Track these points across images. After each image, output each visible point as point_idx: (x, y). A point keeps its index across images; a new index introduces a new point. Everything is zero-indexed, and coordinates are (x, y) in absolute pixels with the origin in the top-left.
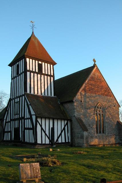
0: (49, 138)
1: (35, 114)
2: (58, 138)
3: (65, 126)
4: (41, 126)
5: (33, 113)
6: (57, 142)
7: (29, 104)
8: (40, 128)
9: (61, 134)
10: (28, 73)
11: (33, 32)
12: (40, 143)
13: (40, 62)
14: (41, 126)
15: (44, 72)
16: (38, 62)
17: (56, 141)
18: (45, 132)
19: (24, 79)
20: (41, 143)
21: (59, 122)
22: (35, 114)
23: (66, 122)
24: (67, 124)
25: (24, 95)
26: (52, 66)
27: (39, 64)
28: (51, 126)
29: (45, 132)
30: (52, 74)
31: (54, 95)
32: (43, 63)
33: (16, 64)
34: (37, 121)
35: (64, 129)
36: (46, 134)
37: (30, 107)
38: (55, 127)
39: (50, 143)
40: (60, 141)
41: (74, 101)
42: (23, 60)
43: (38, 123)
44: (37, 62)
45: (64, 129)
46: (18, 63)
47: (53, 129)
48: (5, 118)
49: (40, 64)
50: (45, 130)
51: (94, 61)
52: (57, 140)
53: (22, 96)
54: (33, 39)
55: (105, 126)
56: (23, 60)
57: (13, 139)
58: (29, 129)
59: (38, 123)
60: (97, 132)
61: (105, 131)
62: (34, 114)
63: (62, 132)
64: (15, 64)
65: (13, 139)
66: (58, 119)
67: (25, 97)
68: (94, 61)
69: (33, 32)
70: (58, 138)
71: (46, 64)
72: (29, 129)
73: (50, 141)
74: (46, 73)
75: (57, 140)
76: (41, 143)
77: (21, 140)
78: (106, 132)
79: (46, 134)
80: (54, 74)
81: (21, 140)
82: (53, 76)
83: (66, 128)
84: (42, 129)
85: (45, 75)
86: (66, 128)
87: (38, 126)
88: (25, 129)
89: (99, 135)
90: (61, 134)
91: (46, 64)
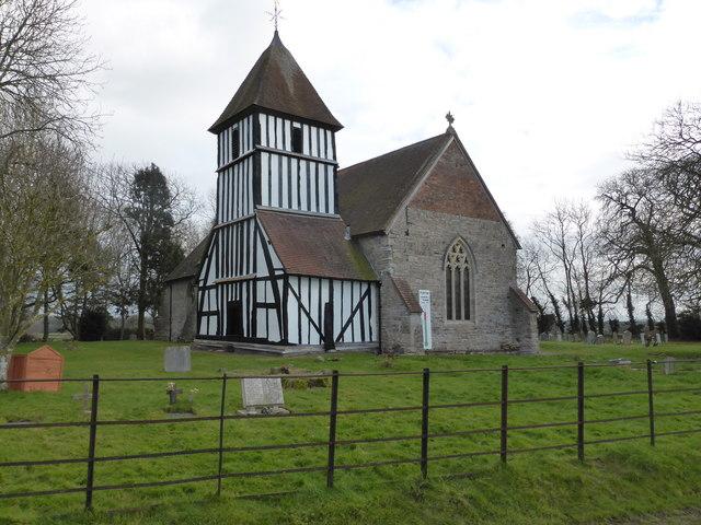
0: (319, 330)
2: (343, 330)
3: (362, 299)
4: (299, 299)
5: (276, 264)
7: (267, 239)
9: (351, 320)
10: (264, 156)
11: (276, 33)
14: (299, 299)
17: (338, 339)
18: (308, 315)
23: (364, 289)
24: (368, 292)
25: (255, 217)
26: (329, 133)
28: (325, 299)
29: (308, 315)
30: (330, 157)
35: (360, 306)
36: (310, 320)
42: (251, 117)
45: (360, 306)
46: (235, 126)
47: (330, 307)
48: (202, 276)
49: (297, 129)
51: (450, 118)
52: (341, 335)
56: (251, 117)
58: (267, 306)
60: (450, 317)
63: (353, 313)
67: (257, 227)
69: (276, 33)
70: (343, 330)
72: (267, 306)
73: (321, 337)
75: (341, 335)
79: (310, 320)
80: (335, 157)
83: (365, 302)
84: (301, 306)
85: (308, 160)
86: (365, 302)
87: (291, 297)
88: (257, 305)
90: (351, 320)
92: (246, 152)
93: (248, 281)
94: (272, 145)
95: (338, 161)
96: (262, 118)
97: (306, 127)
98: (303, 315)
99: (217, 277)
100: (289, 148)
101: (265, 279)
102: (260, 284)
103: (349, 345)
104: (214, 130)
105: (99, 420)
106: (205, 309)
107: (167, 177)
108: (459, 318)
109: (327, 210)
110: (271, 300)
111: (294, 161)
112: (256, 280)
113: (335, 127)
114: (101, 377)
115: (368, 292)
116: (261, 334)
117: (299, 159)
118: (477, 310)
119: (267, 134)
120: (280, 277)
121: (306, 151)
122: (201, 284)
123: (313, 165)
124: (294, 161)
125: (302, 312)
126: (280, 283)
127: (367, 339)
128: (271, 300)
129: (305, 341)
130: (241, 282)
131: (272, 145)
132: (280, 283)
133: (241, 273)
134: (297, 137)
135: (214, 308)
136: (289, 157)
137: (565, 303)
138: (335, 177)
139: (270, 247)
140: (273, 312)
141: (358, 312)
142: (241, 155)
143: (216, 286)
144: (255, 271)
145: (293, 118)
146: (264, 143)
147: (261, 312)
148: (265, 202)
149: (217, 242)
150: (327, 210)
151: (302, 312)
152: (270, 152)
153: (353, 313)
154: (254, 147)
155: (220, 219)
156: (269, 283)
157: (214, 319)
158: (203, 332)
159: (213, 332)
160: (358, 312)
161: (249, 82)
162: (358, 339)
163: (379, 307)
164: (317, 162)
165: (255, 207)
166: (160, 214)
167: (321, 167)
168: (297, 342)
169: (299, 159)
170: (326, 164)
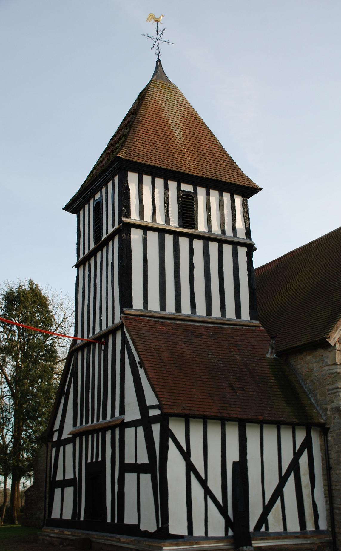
0: (223, 510)
1: (158, 403)
2: (267, 509)
3: (297, 455)
4: (186, 455)
5: (151, 399)
6: (263, 529)
7: (137, 360)
8: (182, 464)
9: (279, 493)
10: (136, 236)
11: (159, 62)
13: (187, 188)
14: (186, 455)
16: (179, 188)
17: (258, 527)
18: (203, 483)
19: (95, 229)
22: (158, 403)
23: (301, 437)
24: (307, 444)
25: (120, 327)
26: (238, 200)
28: (233, 456)
29: (203, 483)
30: (241, 235)
31: (252, 317)
32: (202, 192)
33: (92, 202)
34: (166, 434)
35: (294, 466)
36: (208, 493)
37: (141, 372)
38: (248, 457)
39: (230, 533)
41: (332, 343)
42: (116, 179)
43: (171, 443)
44: (173, 185)
45: (294, 466)
46: (97, 196)
48: (57, 426)
49: (187, 193)
50: (203, 477)
52: (263, 520)
53: (113, 331)
54: (156, 94)
56: (116, 179)
58: (138, 469)
59: (171, 443)
62: (155, 402)
63: (283, 480)
64: (88, 202)
65: (82, 519)
66: (262, 423)
67: (124, 342)
69: (159, 62)
70: (267, 509)
71: (211, 192)
72: (138, 469)
73: (228, 524)
75: (263, 520)
77: (109, 520)
79: (208, 493)
80: (248, 234)
81: (109, 520)
82: (251, 249)
83: (304, 460)
84: (190, 468)
85: (206, 239)
86: (304, 460)
87: (173, 453)
88: (126, 468)
90: (279, 493)
91: (211, 192)
92: (111, 230)
93: (112, 428)
94: (148, 218)
95: (255, 239)
96: (132, 178)
97: (201, 192)
98: (195, 483)
99: (75, 425)
100: (174, 224)
101: (134, 424)
102: (129, 432)
103: (277, 536)
104: (67, 208)
106: (59, 477)
107: (50, 297)
109: (238, 314)
110: (143, 459)
111: (184, 242)
112: (123, 425)
113: (236, 163)
115: (307, 444)
116: (130, 518)
117: (191, 237)
119: (141, 201)
120: (155, 419)
121: (202, 227)
122: (55, 438)
123: (213, 247)
124: (184, 242)
126: (156, 428)
127: (310, 527)
128: (143, 459)
129: (199, 531)
130: (103, 430)
131: (148, 218)
132: (156, 428)
133: (104, 417)
135: (70, 476)
136: (176, 235)
138: (249, 275)
139: (141, 372)
140: (146, 479)
141: (306, 453)
142: (104, 236)
143: (71, 440)
144: (122, 412)
146: (134, 217)
147: (130, 478)
148: (137, 303)
149: (75, 374)
150: (238, 314)
152: (146, 229)
153: (283, 480)
154: (120, 221)
155: (79, 336)
156: (140, 430)
157: (69, 491)
158: (56, 514)
159: (68, 515)
160: (306, 453)
161: (120, 133)
162: (294, 526)
163: (328, 469)
164: (221, 242)
165: (122, 312)
166: (40, 346)
167: (227, 249)
168: (185, 533)
169: (191, 237)
170: (235, 244)
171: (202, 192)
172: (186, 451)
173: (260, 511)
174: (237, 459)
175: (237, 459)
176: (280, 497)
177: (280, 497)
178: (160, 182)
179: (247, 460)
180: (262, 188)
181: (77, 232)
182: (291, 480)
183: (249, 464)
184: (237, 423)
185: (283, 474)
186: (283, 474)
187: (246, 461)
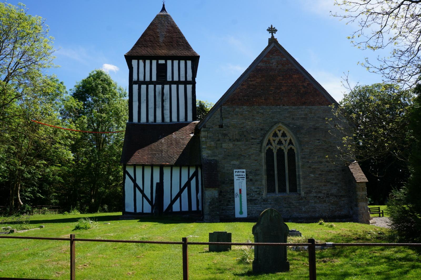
0: (150, 202)
2: (173, 202)
3: (190, 179)
4: (134, 181)
8: (132, 184)
11: (164, 5)
12: (133, 211)
14: (134, 181)
15: (169, 78)
18: (142, 192)
20: (133, 211)
21: (176, 172)
23: (192, 171)
24: (195, 174)
27: (158, 65)
28: (157, 179)
29: (142, 192)
30: (190, 78)
35: (188, 184)
36: (144, 195)
40: (176, 207)
45: (188, 184)
47: (160, 186)
51: (272, 30)
55: (299, 175)
57: (311, 243)
60: (271, 189)
61: (300, 187)
63: (181, 190)
65: (311, 243)
68: (272, 30)
69: (164, 5)
70: (173, 202)
73: (153, 207)
74: (144, 87)
76: (133, 211)
78: (300, 190)
79: (144, 195)
83: (193, 182)
84: (136, 186)
86: (193, 182)
89: (277, 195)
90: (179, 195)
105: (69, 241)
108: (282, 190)
114: (189, 241)
118: (273, 132)
125: (137, 190)
134: (162, 70)
137: (382, 250)
141: (194, 178)
145: (157, 58)
151: (137, 190)
160: (194, 178)
171: (169, 62)
172: (134, 179)
173: (169, 202)
174: (158, 181)
175: (158, 181)
176: (172, 200)
177: (172, 200)
178: (148, 62)
179: (163, 182)
180: (124, 56)
181: (196, 83)
182: (186, 190)
183: (164, 184)
184: (159, 167)
185: (182, 187)
186: (182, 187)
187: (163, 182)
